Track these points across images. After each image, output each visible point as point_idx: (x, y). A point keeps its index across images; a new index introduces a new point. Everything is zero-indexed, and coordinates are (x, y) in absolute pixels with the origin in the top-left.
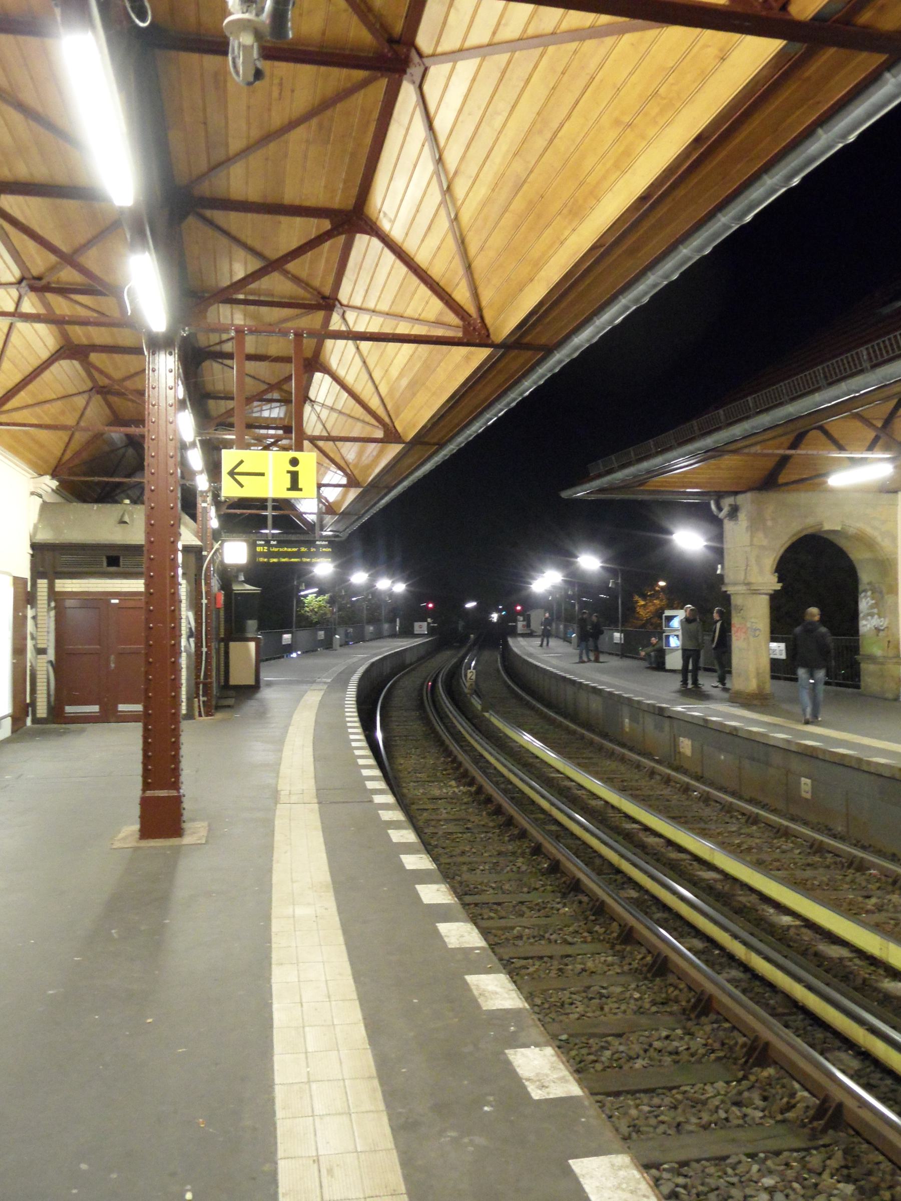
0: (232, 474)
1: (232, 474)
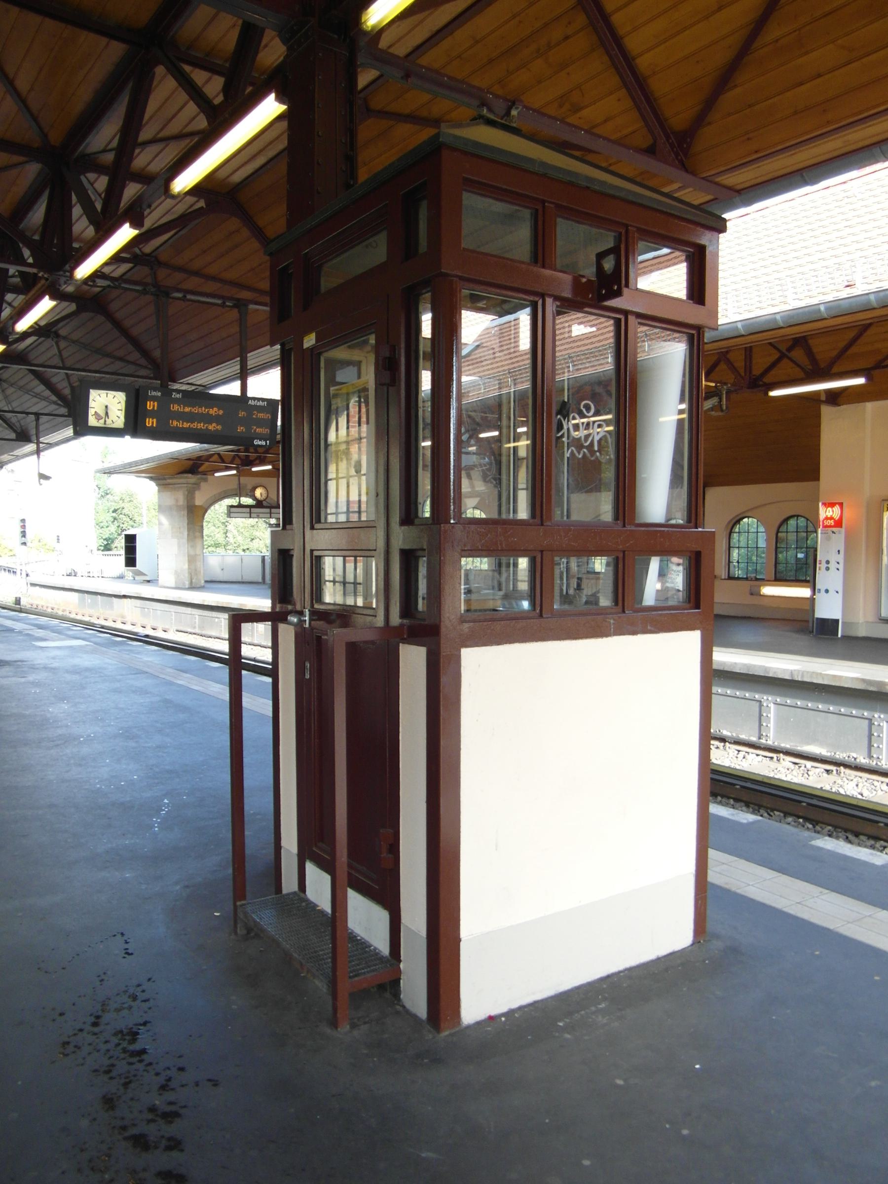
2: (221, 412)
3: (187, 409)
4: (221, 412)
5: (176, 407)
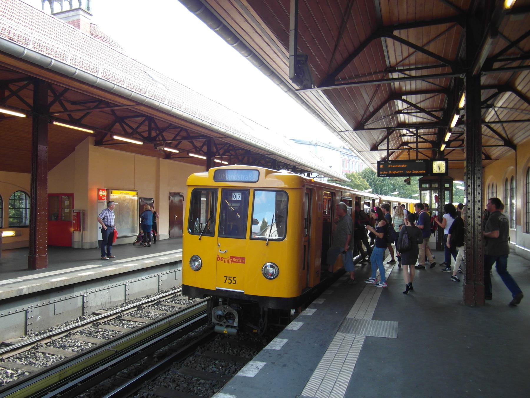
2: (406, 166)
3: (394, 166)
4: (406, 166)
5: (390, 166)
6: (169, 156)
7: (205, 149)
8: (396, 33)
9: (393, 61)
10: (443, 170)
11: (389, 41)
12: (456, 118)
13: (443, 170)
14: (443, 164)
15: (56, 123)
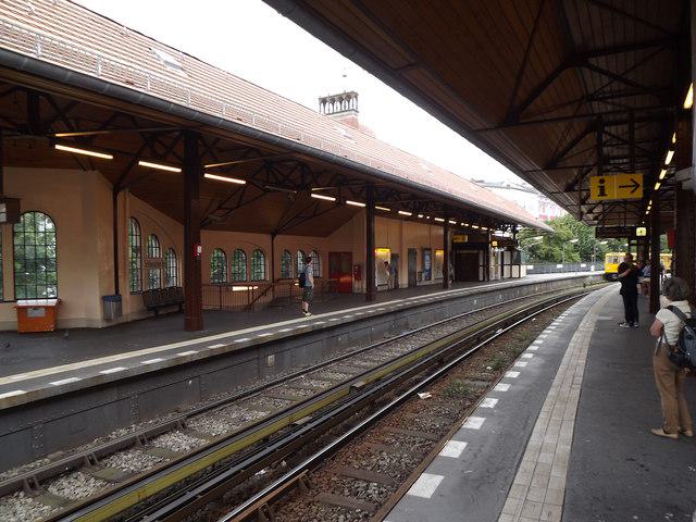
0: (637, 186)
1: (637, 186)
6: (407, 218)
7: (364, 194)
8: (593, 61)
9: (591, 91)
10: (644, 234)
11: (586, 71)
12: (670, 154)
13: (644, 234)
14: (644, 229)
15: (207, 175)
